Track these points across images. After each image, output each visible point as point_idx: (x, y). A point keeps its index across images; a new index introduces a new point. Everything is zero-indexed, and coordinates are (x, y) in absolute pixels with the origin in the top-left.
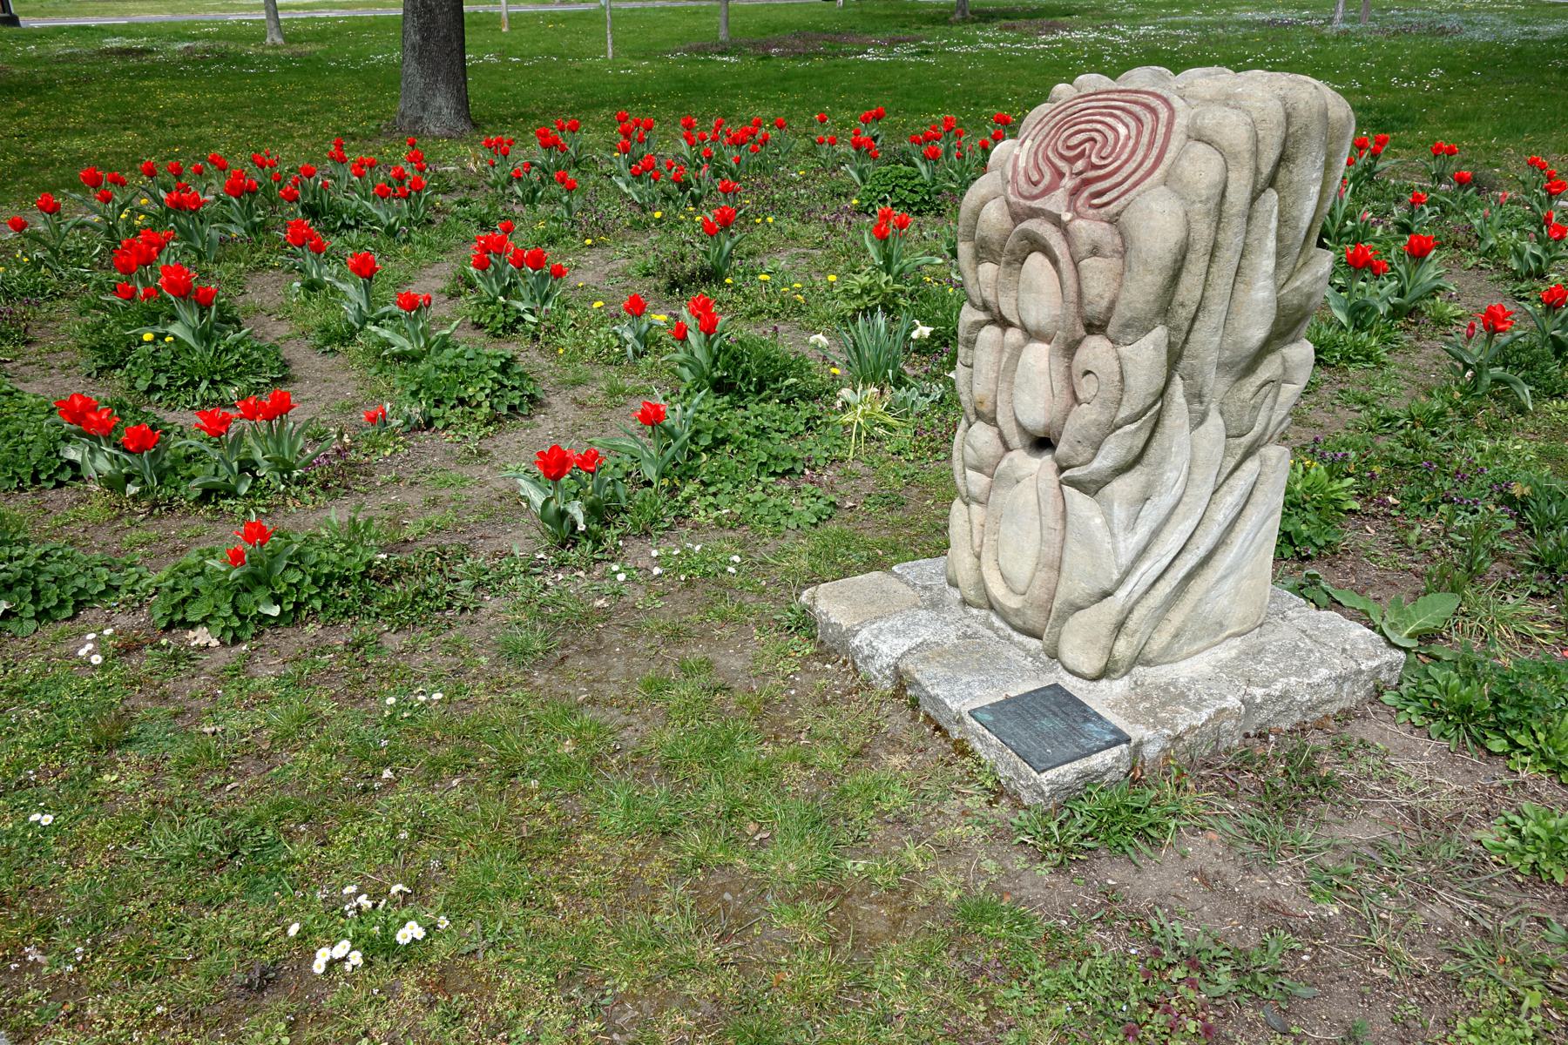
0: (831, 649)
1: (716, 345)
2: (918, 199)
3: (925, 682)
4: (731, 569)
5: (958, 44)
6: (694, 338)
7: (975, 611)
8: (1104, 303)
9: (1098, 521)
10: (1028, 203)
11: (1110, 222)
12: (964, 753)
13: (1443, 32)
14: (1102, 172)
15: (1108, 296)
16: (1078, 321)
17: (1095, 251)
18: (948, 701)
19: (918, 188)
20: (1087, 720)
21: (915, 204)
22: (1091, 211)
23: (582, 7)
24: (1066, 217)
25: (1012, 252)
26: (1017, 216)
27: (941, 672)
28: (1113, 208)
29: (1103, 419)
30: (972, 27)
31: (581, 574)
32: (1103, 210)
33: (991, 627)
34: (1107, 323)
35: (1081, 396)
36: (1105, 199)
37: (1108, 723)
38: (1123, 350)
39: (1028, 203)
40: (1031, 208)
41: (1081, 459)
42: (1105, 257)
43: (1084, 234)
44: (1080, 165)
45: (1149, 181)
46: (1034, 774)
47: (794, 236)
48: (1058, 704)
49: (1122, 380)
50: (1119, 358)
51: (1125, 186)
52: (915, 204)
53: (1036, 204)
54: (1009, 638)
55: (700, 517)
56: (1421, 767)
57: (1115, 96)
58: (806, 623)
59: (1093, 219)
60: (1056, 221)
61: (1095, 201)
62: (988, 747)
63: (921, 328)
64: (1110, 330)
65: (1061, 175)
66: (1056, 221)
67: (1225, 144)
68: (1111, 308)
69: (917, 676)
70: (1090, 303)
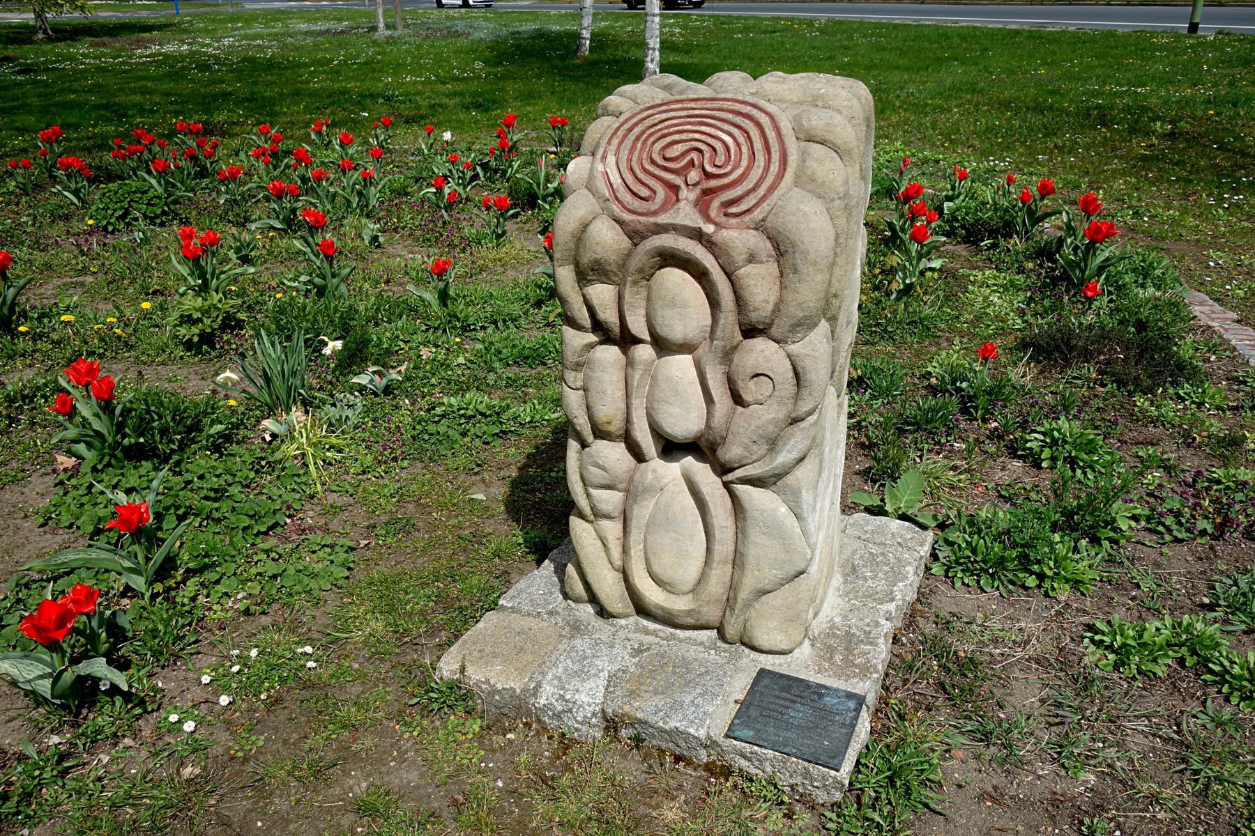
0: (512, 714)
1: (118, 411)
2: (159, 211)
3: (652, 719)
4: (311, 664)
5: (59, 61)
6: (86, 410)
7: (623, 622)
8: (770, 307)
9: (783, 509)
10: (652, 220)
11: (756, 229)
12: (727, 772)
13: (457, 34)
14: (726, 181)
15: (773, 299)
16: (737, 327)
17: (752, 259)
18: (692, 731)
19: (155, 201)
20: (821, 696)
21: (157, 217)
22: (733, 221)
23: (1124, 23)
24: (709, 229)
25: (640, 271)
26: (635, 236)
27: (658, 701)
28: (758, 214)
29: (781, 416)
30: (62, 45)
31: (128, 741)
32: (747, 218)
33: (647, 632)
34: (770, 325)
35: (747, 397)
36: (744, 206)
37: (836, 690)
38: (792, 348)
39: (652, 220)
40: (657, 225)
41: (754, 457)
42: (761, 262)
43: (738, 243)
44: (694, 175)
45: (783, 184)
46: (833, 773)
47: (48, 267)
48: (783, 689)
49: (797, 375)
50: (789, 356)
51: (762, 191)
52: (157, 217)
53: (663, 219)
54: (673, 636)
55: (218, 614)
56: (1005, 625)
57: (692, 105)
58: (459, 695)
59: (739, 227)
60: (698, 235)
61: (733, 210)
62: (763, 761)
63: (331, 344)
64: (774, 331)
65: (675, 189)
66: (698, 235)
67: (839, 142)
68: (777, 309)
69: (640, 715)
70: (756, 309)
